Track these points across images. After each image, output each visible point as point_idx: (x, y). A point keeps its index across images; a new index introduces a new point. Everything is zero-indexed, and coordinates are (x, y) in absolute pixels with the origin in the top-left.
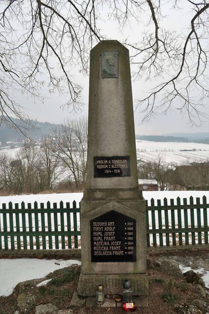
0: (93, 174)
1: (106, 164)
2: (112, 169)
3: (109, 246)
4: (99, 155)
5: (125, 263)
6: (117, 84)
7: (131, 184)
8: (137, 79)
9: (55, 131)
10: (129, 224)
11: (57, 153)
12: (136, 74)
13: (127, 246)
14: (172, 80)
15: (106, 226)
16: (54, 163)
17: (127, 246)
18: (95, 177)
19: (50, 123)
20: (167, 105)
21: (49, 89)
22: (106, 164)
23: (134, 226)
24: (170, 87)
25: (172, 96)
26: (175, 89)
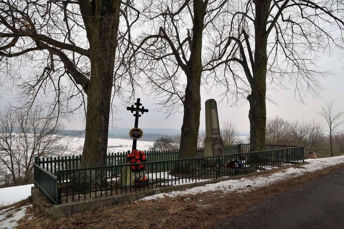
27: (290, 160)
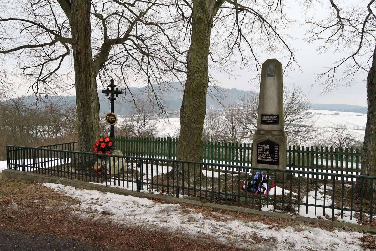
0: (260, 122)
1: (267, 118)
2: (270, 121)
3: (265, 156)
4: (264, 114)
5: (273, 165)
6: (274, 79)
7: (279, 128)
8: (323, 52)
9: (243, 100)
10: (276, 146)
11: (245, 124)
12: (323, 48)
13: (275, 157)
14: (352, 56)
15: (265, 147)
16: (240, 134)
17: (275, 157)
18: (261, 124)
19: (237, 89)
20: (350, 77)
21: (240, 67)
22: (267, 118)
23: (278, 148)
24: (351, 61)
25: (355, 69)
26: (356, 63)
27: (53, 156)
